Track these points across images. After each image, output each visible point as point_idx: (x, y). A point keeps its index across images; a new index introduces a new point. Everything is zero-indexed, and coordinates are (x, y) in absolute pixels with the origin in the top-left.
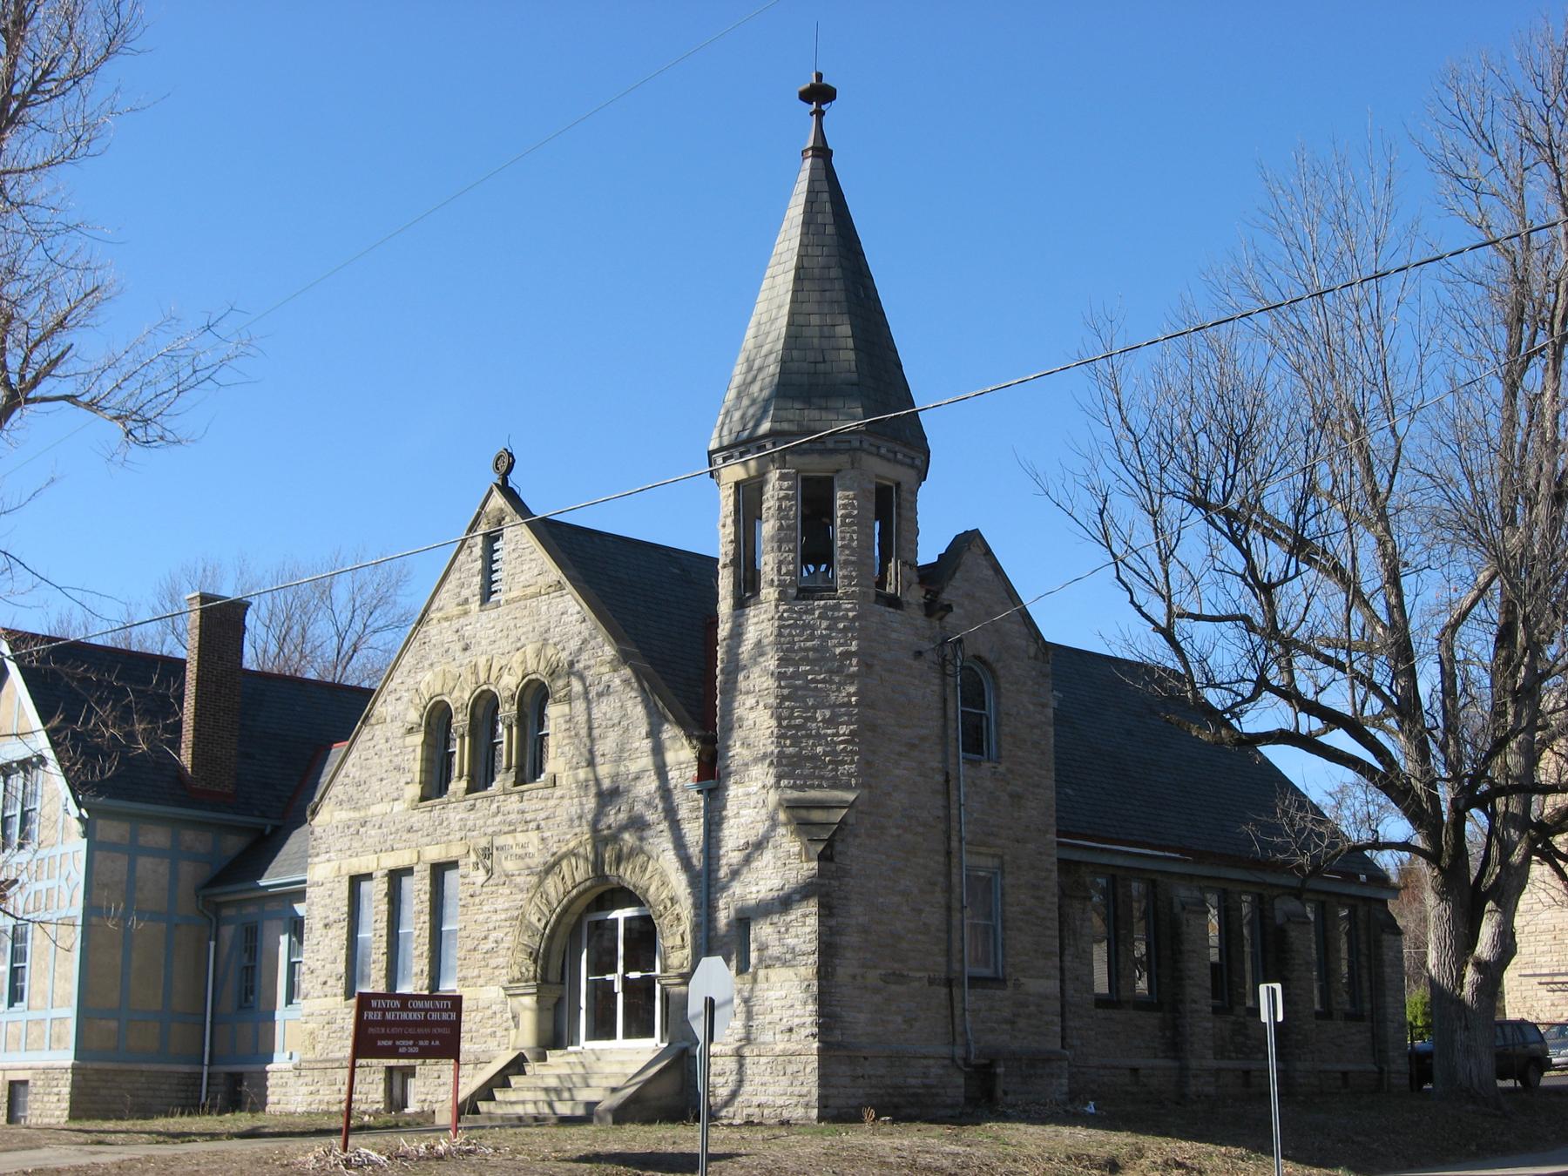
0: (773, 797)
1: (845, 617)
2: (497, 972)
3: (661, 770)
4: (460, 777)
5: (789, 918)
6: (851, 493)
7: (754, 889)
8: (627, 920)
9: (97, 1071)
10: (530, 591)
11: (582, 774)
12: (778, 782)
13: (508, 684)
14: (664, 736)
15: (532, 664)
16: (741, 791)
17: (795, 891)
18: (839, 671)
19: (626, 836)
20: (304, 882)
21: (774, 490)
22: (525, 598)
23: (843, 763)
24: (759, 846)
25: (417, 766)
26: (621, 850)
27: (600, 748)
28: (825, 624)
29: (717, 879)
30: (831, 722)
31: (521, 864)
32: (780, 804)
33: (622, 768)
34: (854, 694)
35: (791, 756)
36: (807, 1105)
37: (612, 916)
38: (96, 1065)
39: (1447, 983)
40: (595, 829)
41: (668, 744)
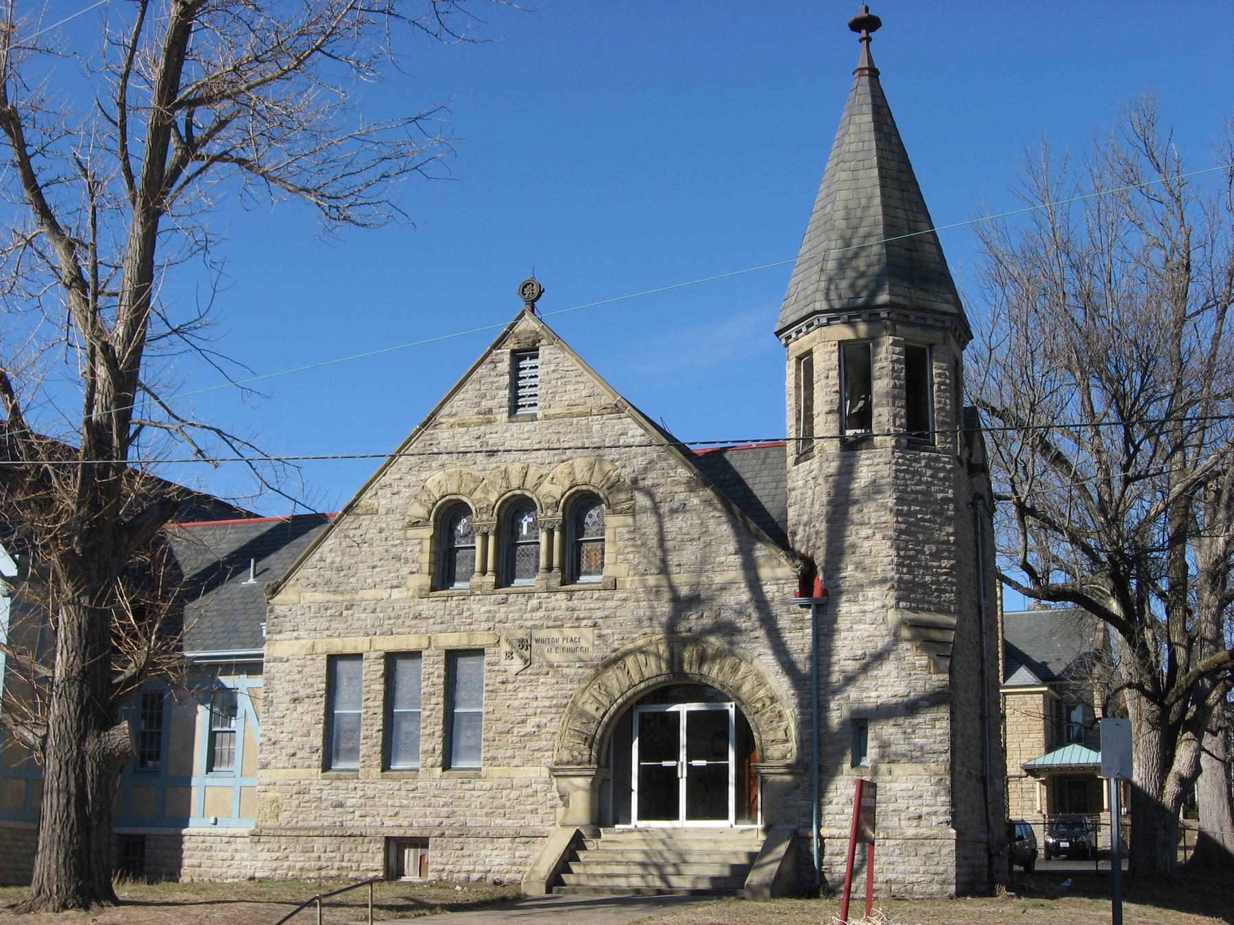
0: (893, 616)
1: (943, 469)
2: (538, 754)
3: (754, 584)
4: (484, 572)
5: (916, 721)
6: (945, 365)
7: (874, 694)
8: (690, 714)
9: (11, 830)
10: (575, 410)
11: (652, 580)
12: (898, 603)
13: (552, 490)
14: (758, 553)
15: (581, 475)
16: (855, 608)
17: (923, 698)
18: (940, 514)
19: (712, 639)
20: (262, 656)
21: (886, 355)
22: (571, 415)
23: (945, 591)
24: (880, 657)
25: (426, 558)
26: (704, 651)
27: (673, 559)
28: (929, 472)
29: (828, 683)
30: (936, 556)
31: (571, 657)
32: (903, 623)
33: (704, 579)
34: (952, 534)
35: (907, 582)
36: (943, 882)
37: (673, 708)
38: (11, 824)
39: (1151, 790)
40: (671, 629)
41: (761, 561)
